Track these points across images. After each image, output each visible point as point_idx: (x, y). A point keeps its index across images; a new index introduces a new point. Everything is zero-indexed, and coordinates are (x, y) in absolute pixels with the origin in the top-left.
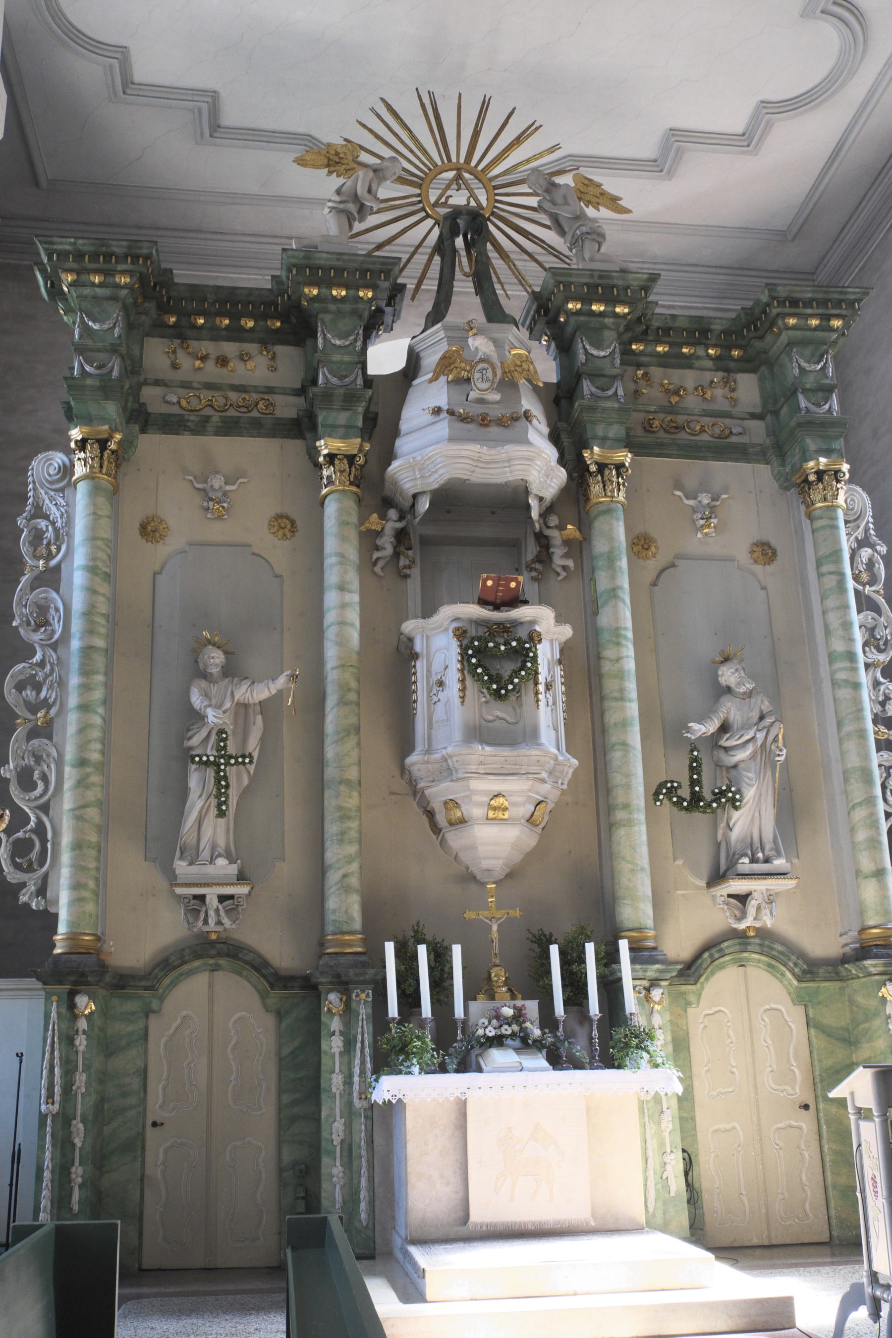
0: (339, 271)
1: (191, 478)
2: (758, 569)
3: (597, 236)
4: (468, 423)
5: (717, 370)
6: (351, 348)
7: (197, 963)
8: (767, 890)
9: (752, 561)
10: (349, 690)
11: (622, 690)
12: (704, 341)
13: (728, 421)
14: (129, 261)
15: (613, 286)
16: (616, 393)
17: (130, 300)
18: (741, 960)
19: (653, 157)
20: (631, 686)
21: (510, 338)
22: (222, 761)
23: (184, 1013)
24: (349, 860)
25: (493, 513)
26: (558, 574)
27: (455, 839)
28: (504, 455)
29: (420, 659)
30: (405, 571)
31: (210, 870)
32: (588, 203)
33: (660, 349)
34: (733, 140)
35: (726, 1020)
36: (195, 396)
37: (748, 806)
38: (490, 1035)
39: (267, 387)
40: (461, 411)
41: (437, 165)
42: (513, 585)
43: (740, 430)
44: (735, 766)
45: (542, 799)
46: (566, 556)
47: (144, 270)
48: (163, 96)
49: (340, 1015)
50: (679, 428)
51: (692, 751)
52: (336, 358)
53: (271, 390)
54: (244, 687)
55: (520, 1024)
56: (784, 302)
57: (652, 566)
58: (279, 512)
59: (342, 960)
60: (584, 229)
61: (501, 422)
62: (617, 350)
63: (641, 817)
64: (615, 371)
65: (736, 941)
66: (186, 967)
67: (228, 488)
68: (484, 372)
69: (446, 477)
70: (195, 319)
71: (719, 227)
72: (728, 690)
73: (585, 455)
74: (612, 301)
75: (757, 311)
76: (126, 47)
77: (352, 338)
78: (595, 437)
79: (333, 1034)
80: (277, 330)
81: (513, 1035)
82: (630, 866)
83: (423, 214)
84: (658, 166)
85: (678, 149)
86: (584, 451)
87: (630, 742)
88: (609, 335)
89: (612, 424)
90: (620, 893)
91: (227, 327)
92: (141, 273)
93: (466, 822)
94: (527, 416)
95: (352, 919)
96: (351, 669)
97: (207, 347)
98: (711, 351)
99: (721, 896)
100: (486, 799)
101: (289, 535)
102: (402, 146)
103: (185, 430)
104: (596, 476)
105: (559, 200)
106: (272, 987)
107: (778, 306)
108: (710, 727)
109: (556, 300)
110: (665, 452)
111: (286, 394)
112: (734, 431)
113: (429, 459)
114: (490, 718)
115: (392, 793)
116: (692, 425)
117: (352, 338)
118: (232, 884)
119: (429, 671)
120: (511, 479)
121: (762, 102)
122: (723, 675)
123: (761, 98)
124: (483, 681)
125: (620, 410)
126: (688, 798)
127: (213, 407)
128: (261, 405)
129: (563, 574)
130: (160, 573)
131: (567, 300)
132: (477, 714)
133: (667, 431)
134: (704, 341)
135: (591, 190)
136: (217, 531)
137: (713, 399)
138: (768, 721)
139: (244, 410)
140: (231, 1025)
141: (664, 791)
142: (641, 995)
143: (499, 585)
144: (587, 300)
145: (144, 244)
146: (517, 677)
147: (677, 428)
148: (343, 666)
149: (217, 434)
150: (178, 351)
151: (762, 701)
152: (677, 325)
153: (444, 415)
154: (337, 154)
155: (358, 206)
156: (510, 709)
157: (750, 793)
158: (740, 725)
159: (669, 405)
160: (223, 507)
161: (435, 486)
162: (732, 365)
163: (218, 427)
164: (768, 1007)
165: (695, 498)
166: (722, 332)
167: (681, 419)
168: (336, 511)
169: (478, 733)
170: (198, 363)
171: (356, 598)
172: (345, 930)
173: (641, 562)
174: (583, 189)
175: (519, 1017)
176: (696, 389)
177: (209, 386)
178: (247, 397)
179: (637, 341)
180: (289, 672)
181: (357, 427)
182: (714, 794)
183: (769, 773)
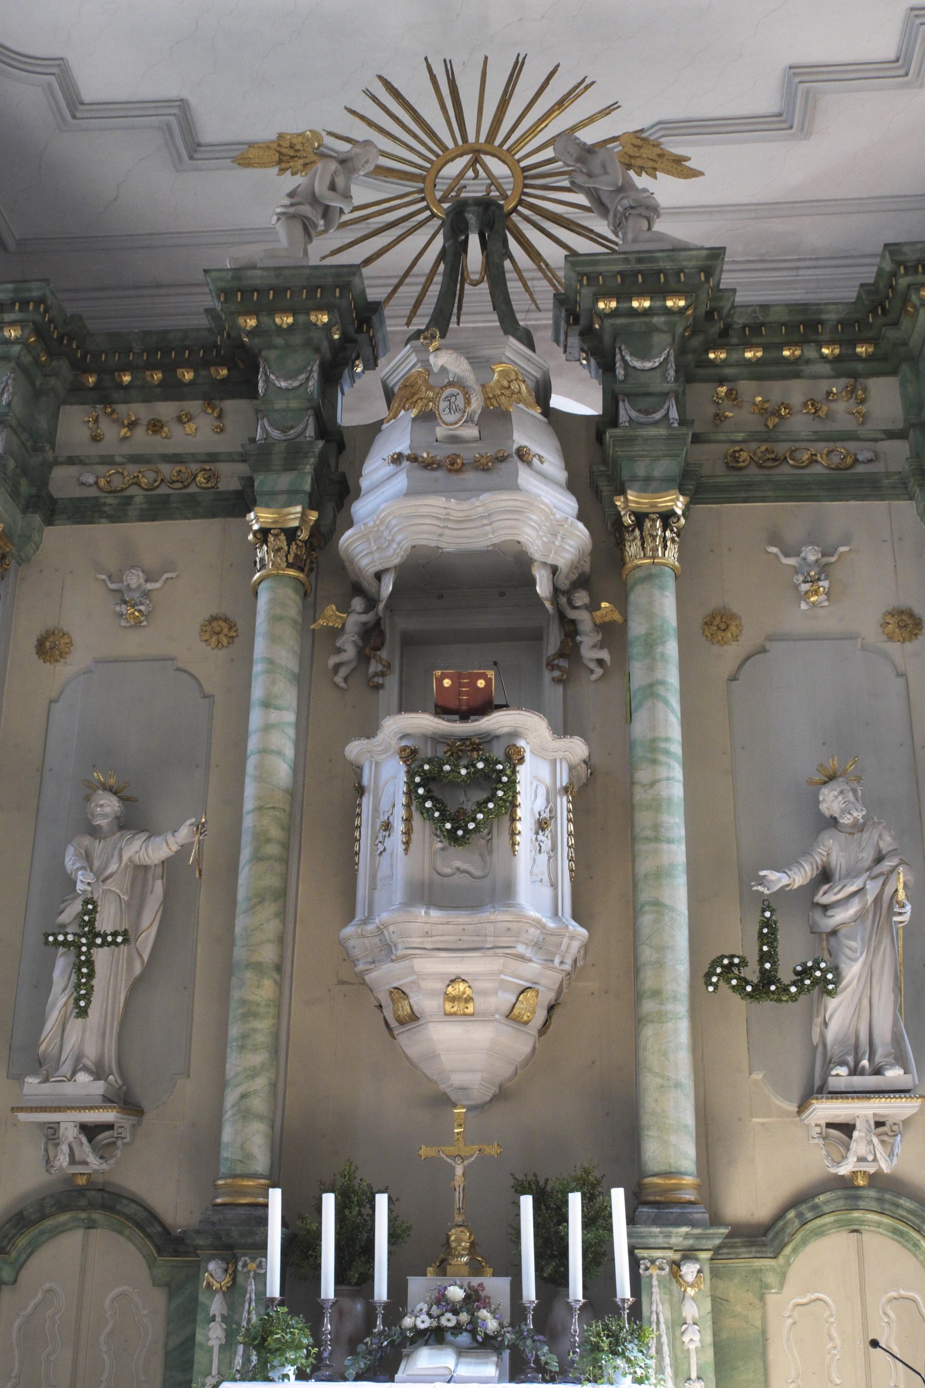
0: (280, 291)
1: (104, 577)
2: (893, 648)
3: (648, 210)
4: (433, 469)
5: (839, 376)
6: (301, 390)
7: (64, 1218)
8: (875, 1115)
9: (885, 637)
10: (268, 840)
11: (656, 827)
12: (814, 337)
13: (852, 446)
14: (17, 308)
15: (660, 271)
16: (666, 415)
17: (27, 359)
18: (849, 1222)
19: (775, 109)
20: (675, 823)
21: (507, 354)
22: (84, 940)
23: (48, 1285)
24: (253, 1073)
25: (502, 594)
26: (592, 672)
27: (411, 1044)
28: (480, 509)
29: (366, 794)
30: (376, 679)
31: (68, 1089)
32: (640, 170)
33: (748, 355)
34: (880, 69)
35: (827, 1313)
36: (118, 472)
37: (850, 989)
38: (422, 1326)
39: (208, 454)
40: (425, 455)
41: (447, 149)
42: (481, 683)
43: (869, 455)
44: (834, 933)
45: (528, 985)
46: (601, 645)
47: (38, 318)
48: (118, 114)
49: (224, 1293)
50: (780, 460)
51: (764, 911)
52: (279, 404)
53: (213, 458)
54: (137, 843)
55: (472, 1313)
56: (916, 267)
57: (733, 652)
58: (214, 611)
59: (230, 1214)
60: (626, 202)
61: (483, 466)
62: (672, 358)
63: (682, 1008)
64: (666, 387)
65: (839, 1193)
66: (50, 1223)
67: (149, 586)
68: (453, 399)
69: (406, 545)
70: (120, 376)
71: (893, 197)
72: (833, 822)
73: (618, 503)
74: (659, 292)
75: (881, 286)
76: (62, 59)
77: (302, 377)
78: (634, 479)
79: (213, 1319)
80: (224, 381)
81: (457, 1329)
82: (659, 1080)
83: (428, 213)
84: (784, 122)
85: (808, 92)
86: (616, 498)
87: (666, 901)
88: (660, 339)
89: (658, 458)
90: (646, 1120)
91: (161, 384)
92: (34, 323)
93: (417, 1019)
94: (523, 455)
95: (249, 1156)
96: (272, 812)
97: (139, 410)
98: (825, 351)
99: (817, 1125)
100: (440, 986)
101: (225, 641)
102: (400, 129)
103: (101, 517)
104: (633, 530)
105: (597, 170)
106: (160, 1251)
107: (906, 274)
108: (799, 877)
109: (584, 301)
110: (757, 494)
111: (233, 461)
112: (860, 458)
113: (382, 523)
114: (448, 871)
115: (342, 982)
116: (797, 455)
117: (302, 377)
118: (97, 1108)
119: (376, 810)
120: (496, 541)
121: (912, 9)
122: (824, 800)
123: (911, 5)
124: (433, 818)
125: (669, 438)
126: (756, 981)
127: (140, 486)
128: (200, 478)
129: (599, 671)
130: (56, 701)
131: (596, 298)
132: (427, 866)
133: (760, 466)
134: (814, 337)
135: (645, 152)
136: (134, 643)
137: (829, 416)
138: (887, 864)
139: (179, 485)
140: (107, 1303)
141: (719, 970)
142: (663, 1273)
143: (461, 685)
144: (623, 296)
145: (34, 285)
146: (481, 812)
147: (775, 460)
148: (260, 808)
149: (142, 518)
150: (101, 419)
151: (880, 836)
152: (772, 318)
153: (406, 463)
154: (292, 146)
155: (320, 210)
156: (477, 857)
157: (852, 971)
158: (843, 872)
159: (765, 429)
160: (140, 611)
161: (396, 561)
162: (860, 367)
163: (141, 509)
164: (894, 1294)
165: (798, 554)
166: (839, 322)
167: (782, 448)
168: (272, 603)
169: (428, 893)
170: (124, 431)
171: (290, 717)
172: (238, 1172)
173: (715, 648)
174: (633, 151)
175: (474, 1299)
176: (805, 405)
177: (135, 459)
178: (183, 469)
179: (716, 347)
180: (193, 820)
181: (304, 492)
182: (797, 973)
183: (886, 942)
